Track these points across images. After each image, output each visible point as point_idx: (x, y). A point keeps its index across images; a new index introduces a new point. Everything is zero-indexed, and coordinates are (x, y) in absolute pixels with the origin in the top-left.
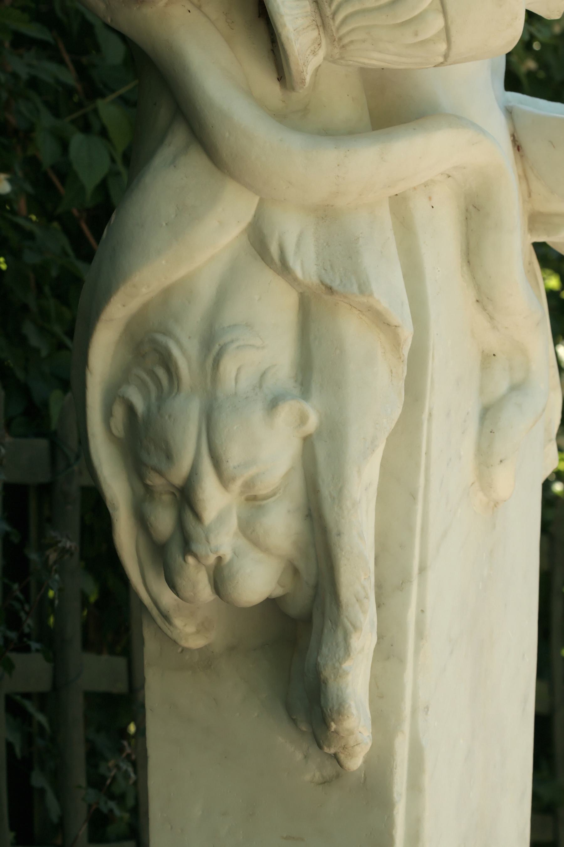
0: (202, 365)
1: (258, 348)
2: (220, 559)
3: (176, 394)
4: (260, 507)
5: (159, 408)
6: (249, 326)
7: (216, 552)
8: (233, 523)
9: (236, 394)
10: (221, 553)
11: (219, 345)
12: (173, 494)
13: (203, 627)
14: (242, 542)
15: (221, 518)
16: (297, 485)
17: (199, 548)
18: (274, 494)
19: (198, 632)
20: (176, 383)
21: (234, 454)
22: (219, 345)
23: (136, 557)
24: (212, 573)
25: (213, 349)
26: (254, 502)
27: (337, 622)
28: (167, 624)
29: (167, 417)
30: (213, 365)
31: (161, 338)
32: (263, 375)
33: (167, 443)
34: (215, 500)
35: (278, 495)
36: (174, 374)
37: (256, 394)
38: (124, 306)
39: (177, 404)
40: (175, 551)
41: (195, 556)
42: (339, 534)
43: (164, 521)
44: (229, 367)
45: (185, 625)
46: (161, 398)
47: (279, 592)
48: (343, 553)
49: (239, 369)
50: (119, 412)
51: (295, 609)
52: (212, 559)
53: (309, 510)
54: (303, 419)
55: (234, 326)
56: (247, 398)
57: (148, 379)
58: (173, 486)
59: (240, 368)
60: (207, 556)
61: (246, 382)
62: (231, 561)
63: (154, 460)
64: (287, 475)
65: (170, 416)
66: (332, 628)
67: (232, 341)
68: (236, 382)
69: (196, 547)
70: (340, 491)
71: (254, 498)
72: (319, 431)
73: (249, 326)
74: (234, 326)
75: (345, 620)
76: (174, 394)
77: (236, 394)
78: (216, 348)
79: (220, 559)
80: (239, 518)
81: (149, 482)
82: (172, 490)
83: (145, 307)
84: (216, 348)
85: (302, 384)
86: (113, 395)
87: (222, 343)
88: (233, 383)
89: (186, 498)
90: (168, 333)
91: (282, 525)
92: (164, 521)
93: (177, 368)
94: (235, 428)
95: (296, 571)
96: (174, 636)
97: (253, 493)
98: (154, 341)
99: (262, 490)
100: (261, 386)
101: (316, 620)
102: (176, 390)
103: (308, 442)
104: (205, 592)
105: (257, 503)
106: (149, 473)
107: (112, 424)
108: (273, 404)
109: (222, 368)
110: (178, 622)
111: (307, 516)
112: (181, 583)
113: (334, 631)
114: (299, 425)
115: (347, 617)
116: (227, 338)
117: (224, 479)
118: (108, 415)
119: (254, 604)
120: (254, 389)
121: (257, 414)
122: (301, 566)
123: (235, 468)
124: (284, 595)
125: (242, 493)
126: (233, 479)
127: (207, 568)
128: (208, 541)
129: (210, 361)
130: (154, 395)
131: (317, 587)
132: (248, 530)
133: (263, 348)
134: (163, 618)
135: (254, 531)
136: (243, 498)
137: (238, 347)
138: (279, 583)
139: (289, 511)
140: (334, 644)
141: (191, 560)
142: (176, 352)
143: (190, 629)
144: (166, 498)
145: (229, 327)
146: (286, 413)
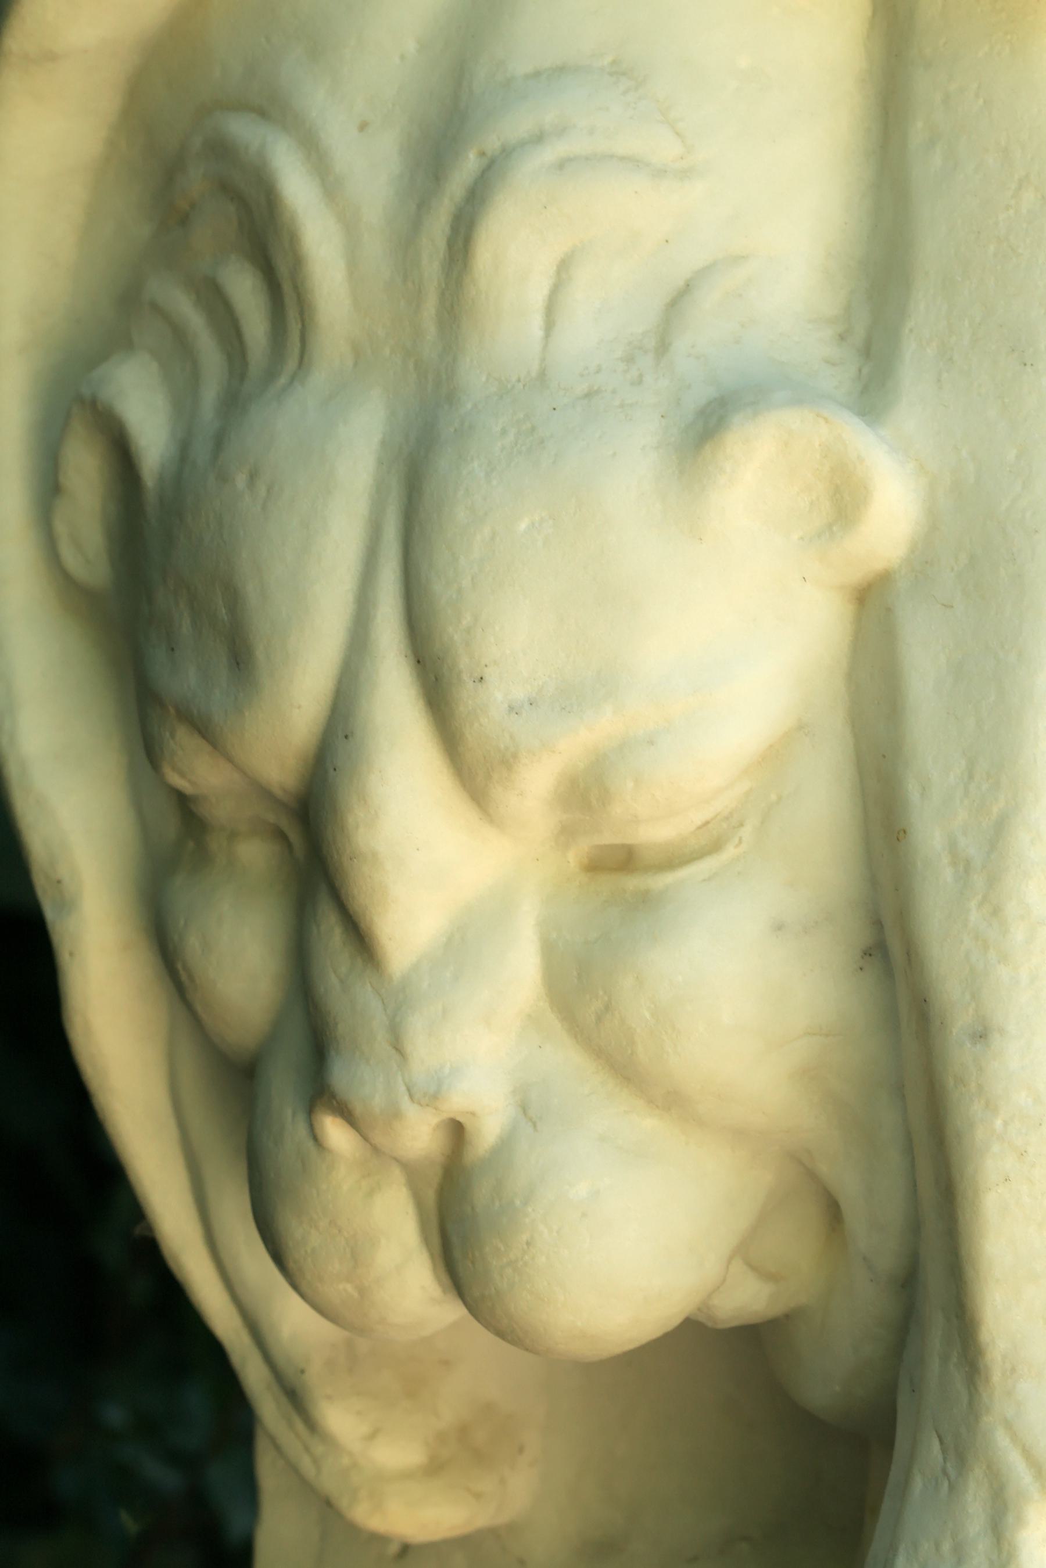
0: (406, 243)
1: (660, 173)
4: (645, 902)
5: (219, 442)
6: (624, 73)
7: (432, 1098)
8: (520, 970)
9: (542, 377)
11: (482, 154)
12: (280, 835)
13: (465, 1450)
14: (563, 1060)
15: (464, 944)
16: (820, 803)
19: (434, 1468)
21: (512, 644)
22: (482, 154)
23: (171, 1124)
24: (430, 1196)
25: (453, 167)
26: (620, 877)
27: (963, 1448)
28: (300, 1426)
29: (241, 480)
31: (244, 130)
32: (679, 301)
33: (234, 598)
34: (429, 857)
35: (730, 852)
37: (639, 381)
39: (286, 420)
40: (282, 1088)
41: (346, 1114)
42: (982, 1035)
44: (519, 251)
45: (372, 1436)
46: (234, 402)
47: (746, 1299)
48: (998, 1123)
49: (564, 268)
50: (85, 469)
51: (828, 1375)
52: (419, 1135)
53: (878, 924)
54: (844, 500)
55: (557, 74)
56: (589, 395)
58: (264, 792)
59: (565, 263)
61: (597, 323)
62: (505, 1145)
63: (184, 678)
64: (774, 758)
65: (253, 477)
66: (945, 1473)
67: (539, 138)
68: (549, 325)
69: (350, 1076)
70: (998, 834)
71: (620, 861)
72: (922, 560)
73: (624, 73)
74: (557, 74)
75: (1002, 1439)
76: (283, 380)
77: (542, 377)
78: (469, 164)
79: (457, 1131)
80: (549, 950)
82: (271, 818)
85: (867, 351)
87: (492, 143)
88: (537, 321)
90: (273, 107)
91: (743, 988)
92: (241, 955)
93: (298, 262)
94: (523, 526)
96: (328, 1483)
97: (608, 838)
98: (222, 150)
100: (663, 347)
102: (292, 364)
103: (873, 606)
104: (407, 1286)
105: (633, 883)
106: (173, 736)
107: (61, 528)
108: (705, 426)
109: (484, 254)
110: (341, 1419)
111: (867, 953)
112: (305, 1236)
114: (830, 526)
115: (1008, 1425)
116: (515, 125)
117: (473, 769)
119: (618, 1350)
120: (629, 359)
121: (629, 466)
122: (849, 1186)
124: (787, 1316)
125: (566, 834)
127: (412, 1172)
128: (398, 1047)
130: (210, 394)
132: (582, 995)
133: (685, 174)
134: (284, 1400)
135: (608, 1007)
136: (573, 858)
137: (561, 165)
138: (745, 1252)
139: (779, 927)
140: (946, 1547)
141: (335, 1132)
142: (297, 189)
143: (397, 1453)
144: (255, 854)
145: (537, 74)
146: (761, 467)
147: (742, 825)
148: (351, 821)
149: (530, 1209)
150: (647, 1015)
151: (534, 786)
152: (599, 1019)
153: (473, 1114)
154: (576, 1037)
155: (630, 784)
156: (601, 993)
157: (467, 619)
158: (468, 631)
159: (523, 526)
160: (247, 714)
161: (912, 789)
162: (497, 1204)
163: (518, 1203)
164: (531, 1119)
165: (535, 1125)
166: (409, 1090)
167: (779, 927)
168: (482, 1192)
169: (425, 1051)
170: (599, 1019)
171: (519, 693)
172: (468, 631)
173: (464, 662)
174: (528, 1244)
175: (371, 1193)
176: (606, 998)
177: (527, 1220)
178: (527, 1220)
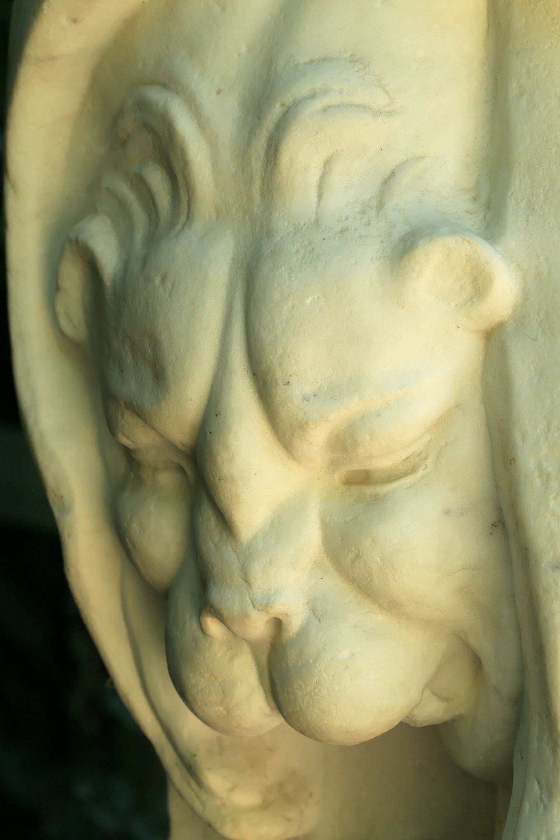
1: (377, 113)
3: (184, 226)
4: (376, 500)
5: (145, 261)
7: (265, 607)
8: (310, 537)
10: (279, 607)
11: (283, 105)
14: (334, 585)
15: (280, 525)
16: (468, 448)
17: (227, 597)
18: (410, 468)
20: (184, 200)
21: (304, 364)
22: (283, 105)
23: (123, 624)
24: (264, 659)
25: (267, 112)
26: (362, 487)
28: (194, 785)
29: (157, 281)
30: (267, 153)
31: (155, 95)
32: (389, 180)
34: (261, 479)
35: (421, 473)
36: (180, 178)
37: (369, 223)
38: (75, 21)
39: (181, 249)
40: (184, 603)
44: (303, 156)
45: (232, 789)
46: (153, 239)
47: (432, 711)
49: (328, 164)
50: (73, 277)
52: (258, 626)
53: (500, 510)
54: (478, 284)
57: (130, 197)
58: (172, 446)
59: (329, 162)
60: (245, 615)
61: (345, 194)
62: (304, 631)
63: (129, 386)
64: (443, 422)
65: (164, 278)
67: (313, 96)
68: (320, 196)
71: (362, 479)
72: (520, 317)
76: (178, 227)
78: (277, 110)
79: (278, 624)
80: (325, 526)
81: (124, 441)
82: (176, 460)
83: (129, 26)
84: (277, 110)
85: (488, 206)
86: (67, 244)
87: (288, 99)
88: (313, 194)
90: (170, 82)
92: (161, 534)
93: (186, 164)
94: (309, 301)
95: (477, 664)
96: (209, 814)
97: (356, 467)
98: (143, 105)
99: (379, 457)
100: (381, 205)
101: (509, 785)
102: (183, 218)
103: (495, 340)
104: (252, 706)
105: (369, 490)
106: (123, 417)
107: (60, 309)
108: (404, 247)
109: (285, 158)
110: (215, 780)
111: (494, 525)
112: (197, 682)
113: (545, 808)
114: (471, 299)
116: (301, 89)
118: (53, 288)
119: (365, 739)
120: (363, 212)
121: (364, 270)
122: (485, 648)
123: (305, 399)
125: (333, 465)
126: (303, 426)
127: (254, 647)
128: (246, 580)
129: (260, 144)
130: (139, 235)
131: (519, 701)
132: (345, 551)
133: (391, 114)
134: (185, 771)
135: (357, 557)
136: (338, 477)
137: (325, 110)
138: (431, 686)
139: (447, 512)
141: (213, 626)
142: (185, 125)
143: (245, 798)
144: (167, 479)
146: (434, 267)
148: (219, 459)
151: (317, 438)
152: (353, 563)
153: (287, 615)
154: (340, 572)
155: (368, 438)
156: (354, 549)
157: (280, 351)
160: (163, 404)
161: (518, 437)
162: (300, 663)
165: (319, 620)
166: (252, 602)
169: (262, 580)
170: (353, 563)
171: (308, 390)
172: (281, 357)
173: (279, 374)
174: (317, 683)
175: (232, 658)
178: (317, 671)
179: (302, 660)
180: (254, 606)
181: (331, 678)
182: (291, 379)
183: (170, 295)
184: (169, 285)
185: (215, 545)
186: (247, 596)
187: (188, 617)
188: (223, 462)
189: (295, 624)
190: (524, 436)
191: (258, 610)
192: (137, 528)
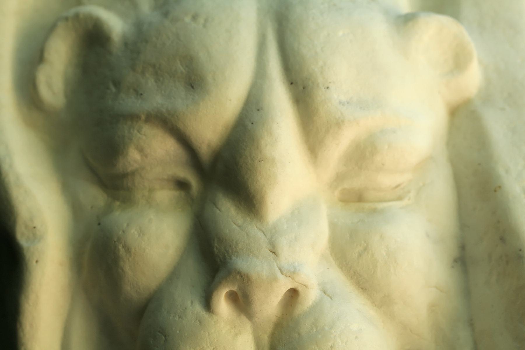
2: (293, 294)
14: (337, 277)
15: (298, 215)
21: (340, 79)
24: (265, 339)
34: (292, 178)
43: (157, 238)
50: (60, 54)
52: (269, 305)
53: (462, 247)
54: (459, 62)
62: (317, 306)
72: (486, 96)
80: (333, 226)
89: (225, 174)
92: (157, 238)
94: (341, 33)
111: (455, 261)
125: (340, 178)
135: (366, 249)
136: (337, 193)
147: (400, 198)
148: (263, 143)
149: (333, 331)
150: (385, 254)
151: (337, 148)
152: (360, 255)
153: (306, 286)
154: (341, 268)
155: (386, 147)
156: (363, 242)
157: (320, 63)
158: (322, 67)
159: (341, 33)
160: (201, 104)
161: (501, 171)
162: (315, 330)
163: (327, 328)
164: (328, 296)
165: (331, 298)
166: (280, 269)
167: (428, 236)
168: (305, 327)
169: (287, 255)
170: (360, 255)
171: (343, 98)
172: (322, 67)
173: (320, 80)
174: (331, 347)
175: (236, 335)
176: (365, 245)
177: (332, 336)
178: (332, 336)
179: (317, 328)
180: (282, 273)
181: (344, 344)
182: (330, 85)
183: (204, 26)
184: (201, 21)
185: (239, 227)
186: (275, 264)
187: (189, 303)
188: (266, 146)
189: (311, 296)
190: (507, 171)
191: (286, 276)
192: (136, 233)
